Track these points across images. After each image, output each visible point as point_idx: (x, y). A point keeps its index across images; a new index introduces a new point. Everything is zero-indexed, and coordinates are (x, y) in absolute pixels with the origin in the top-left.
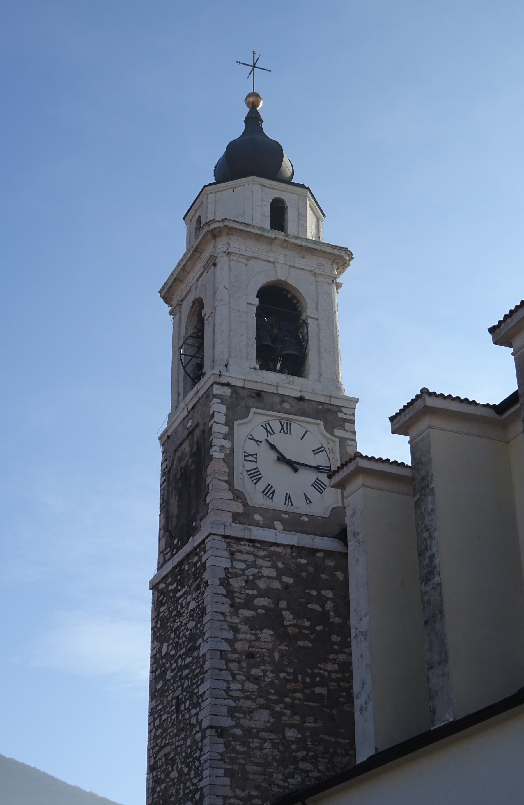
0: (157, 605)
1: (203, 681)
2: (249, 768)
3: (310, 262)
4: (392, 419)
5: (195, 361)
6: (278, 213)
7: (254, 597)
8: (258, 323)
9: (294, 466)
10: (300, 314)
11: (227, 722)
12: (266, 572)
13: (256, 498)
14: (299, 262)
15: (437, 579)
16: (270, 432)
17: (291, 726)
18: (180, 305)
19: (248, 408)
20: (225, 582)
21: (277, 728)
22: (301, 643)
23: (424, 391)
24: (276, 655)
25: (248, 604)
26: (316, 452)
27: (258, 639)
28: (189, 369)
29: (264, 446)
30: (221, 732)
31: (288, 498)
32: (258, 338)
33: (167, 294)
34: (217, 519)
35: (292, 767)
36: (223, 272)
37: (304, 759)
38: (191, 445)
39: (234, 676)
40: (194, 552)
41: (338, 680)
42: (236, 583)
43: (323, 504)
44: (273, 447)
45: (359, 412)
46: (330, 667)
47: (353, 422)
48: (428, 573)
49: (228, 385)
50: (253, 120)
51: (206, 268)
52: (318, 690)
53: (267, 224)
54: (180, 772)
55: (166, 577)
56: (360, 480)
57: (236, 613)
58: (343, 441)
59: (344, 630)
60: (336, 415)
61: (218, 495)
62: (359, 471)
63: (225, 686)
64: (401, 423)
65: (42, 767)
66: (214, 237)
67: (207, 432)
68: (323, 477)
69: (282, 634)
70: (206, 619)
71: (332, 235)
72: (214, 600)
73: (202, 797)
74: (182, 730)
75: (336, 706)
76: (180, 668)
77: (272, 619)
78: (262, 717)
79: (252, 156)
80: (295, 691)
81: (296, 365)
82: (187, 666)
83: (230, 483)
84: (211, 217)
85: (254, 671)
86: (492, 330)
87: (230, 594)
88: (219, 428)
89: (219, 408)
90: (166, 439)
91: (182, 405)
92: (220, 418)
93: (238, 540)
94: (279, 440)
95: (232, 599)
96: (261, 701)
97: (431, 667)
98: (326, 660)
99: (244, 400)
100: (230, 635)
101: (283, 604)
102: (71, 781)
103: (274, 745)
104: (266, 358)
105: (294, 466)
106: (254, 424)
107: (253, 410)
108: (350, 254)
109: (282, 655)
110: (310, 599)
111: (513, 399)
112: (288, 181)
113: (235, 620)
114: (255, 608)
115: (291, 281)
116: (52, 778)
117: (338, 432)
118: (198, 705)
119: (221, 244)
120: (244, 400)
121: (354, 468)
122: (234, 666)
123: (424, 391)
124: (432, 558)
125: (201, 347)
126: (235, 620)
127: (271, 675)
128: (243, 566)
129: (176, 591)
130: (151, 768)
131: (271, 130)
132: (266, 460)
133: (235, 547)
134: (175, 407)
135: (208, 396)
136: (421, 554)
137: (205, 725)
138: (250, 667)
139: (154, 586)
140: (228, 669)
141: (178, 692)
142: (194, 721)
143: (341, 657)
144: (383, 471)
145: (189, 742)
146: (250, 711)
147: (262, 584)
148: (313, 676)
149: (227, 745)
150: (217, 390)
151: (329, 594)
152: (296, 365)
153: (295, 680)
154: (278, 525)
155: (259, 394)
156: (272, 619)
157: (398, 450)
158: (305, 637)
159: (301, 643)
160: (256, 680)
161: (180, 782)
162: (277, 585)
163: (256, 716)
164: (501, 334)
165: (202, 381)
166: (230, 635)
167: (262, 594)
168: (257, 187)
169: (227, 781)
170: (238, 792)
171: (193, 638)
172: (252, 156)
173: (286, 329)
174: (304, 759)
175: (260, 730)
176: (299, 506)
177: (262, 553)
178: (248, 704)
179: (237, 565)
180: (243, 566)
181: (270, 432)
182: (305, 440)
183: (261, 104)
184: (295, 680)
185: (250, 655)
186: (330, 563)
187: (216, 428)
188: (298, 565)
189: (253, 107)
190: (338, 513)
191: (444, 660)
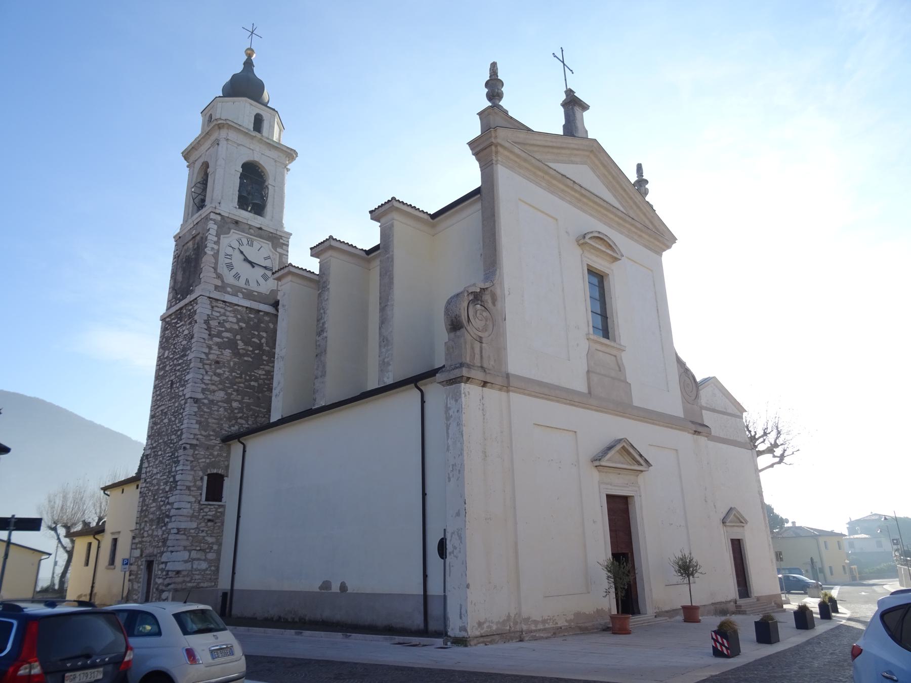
0: (164, 330)
1: (188, 373)
2: (210, 420)
3: (273, 154)
4: (311, 249)
5: (200, 197)
6: (258, 122)
7: (223, 331)
8: (238, 182)
9: (252, 264)
10: (264, 181)
11: (200, 396)
12: (231, 319)
13: (229, 279)
14: (268, 152)
15: (325, 334)
16: (241, 244)
17: (236, 401)
18: (194, 163)
19: (230, 229)
20: (207, 322)
21: (228, 401)
22: (246, 358)
23: (331, 237)
24: (232, 364)
25: (219, 335)
26: (266, 259)
27: (222, 354)
28: (197, 201)
29: (237, 251)
30: (196, 401)
31: (247, 281)
32: (239, 191)
33: (187, 155)
34: (205, 288)
35: (234, 422)
36: (223, 147)
37: (241, 418)
38: (194, 244)
39: (207, 372)
40: (190, 303)
41: (264, 379)
42: (213, 323)
43: (266, 287)
44: (242, 252)
45: (292, 241)
46: (260, 372)
47: (288, 245)
48: (321, 331)
49: (219, 214)
50: (249, 64)
51: (212, 145)
52: (252, 383)
53: (251, 127)
54: (170, 420)
55: (171, 315)
56: (289, 278)
57: (211, 339)
58: (281, 255)
59: (272, 355)
60: (279, 240)
61: (207, 273)
62: (290, 273)
63: (201, 377)
64: (316, 251)
65: (70, 409)
66: (219, 128)
67: (204, 239)
68: (269, 273)
69: (236, 353)
70: (193, 340)
71: (287, 141)
72: (199, 331)
73: (182, 433)
74: (173, 398)
75: (263, 392)
76: (175, 365)
77: (231, 344)
78: (220, 395)
79: (245, 85)
80: (240, 383)
81: (259, 210)
82: (179, 365)
83: (215, 269)
84: (218, 116)
85: (218, 371)
86: (371, 212)
87: (209, 328)
88: (212, 238)
89: (213, 227)
90: (178, 238)
91: (190, 221)
92: (213, 232)
93: (217, 300)
94: (246, 249)
95: (210, 331)
96: (220, 386)
97: (316, 378)
98: (258, 368)
99: (227, 224)
100: (207, 351)
101: (238, 337)
102: (88, 418)
103: (226, 410)
104: (243, 203)
105: (252, 264)
106: (232, 238)
107: (232, 231)
108: (297, 154)
109: (235, 364)
110: (254, 336)
111: (376, 248)
112: (266, 105)
113: (210, 342)
114: (222, 338)
115: (261, 162)
116: (76, 415)
117: (279, 250)
118: (184, 385)
119: (223, 133)
120: (227, 224)
121: (286, 271)
122: (207, 367)
123: (331, 237)
124: (324, 324)
125: (205, 189)
126: (210, 342)
127: (228, 373)
128: (218, 314)
129: (177, 323)
130: (152, 417)
131: (259, 72)
132: (237, 259)
133: (214, 304)
134: (185, 220)
135: (207, 218)
136: (318, 321)
137: (187, 396)
138: (216, 369)
139: (163, 319)
140: (204, 368)
141: (173, 378)
142: (181, 394)
143: (267, 368)
144: (302, 275)
145: (176, 405)
146: (214, 391)
147: (228, 325)
148: (250, 376)
149: (199, 408)
150: (212, 216)
151: (264, 334)
152: (259, 210)
153: (241, 377)
154: (240, 295)
155: (237, 222)
156: (231, 344)
157: (313, 265)
158: (248, 356)
159: (246, 358)
160: (219, 375)
161: (169, 425)
162: (236, 327)
163: (217, 394)
164: (375, 214)
165: (204, 209)
166: (207, 351)
167: (227, 331)
168: (248, 105)
169: (197, 426)
170: (203, 433)
171: (185, 349)
172: (245, 85)
173: (255, 189)
174: (241, 418)
175: (218, 402)
176: (253, 286)
177: (229, 309)
178: (213, 387)
179: (214, 313)
180: (218, 314)
181: (241, 244)
182: (260, 251)
183: (254, 56)
184: (241, 377)
185: (217, 362)
186: (267, 318)
187: (210, 237)
188: (249, 317)
189: (249, 56)
190: (274, 292)
191: (324, 374)
